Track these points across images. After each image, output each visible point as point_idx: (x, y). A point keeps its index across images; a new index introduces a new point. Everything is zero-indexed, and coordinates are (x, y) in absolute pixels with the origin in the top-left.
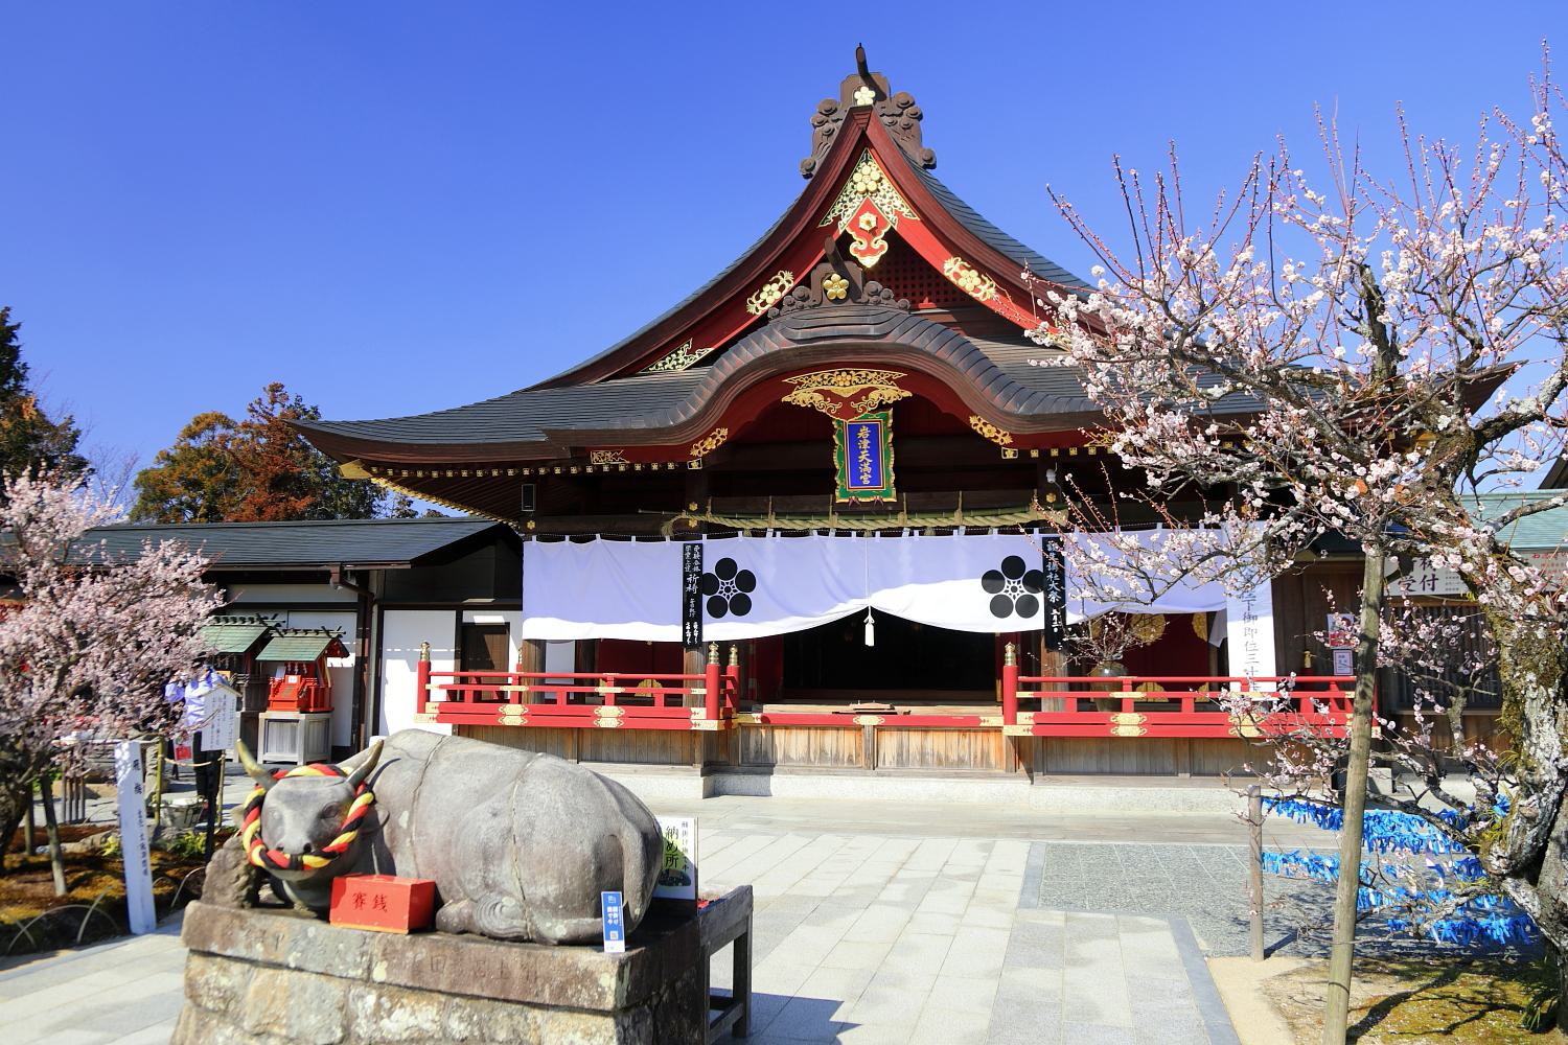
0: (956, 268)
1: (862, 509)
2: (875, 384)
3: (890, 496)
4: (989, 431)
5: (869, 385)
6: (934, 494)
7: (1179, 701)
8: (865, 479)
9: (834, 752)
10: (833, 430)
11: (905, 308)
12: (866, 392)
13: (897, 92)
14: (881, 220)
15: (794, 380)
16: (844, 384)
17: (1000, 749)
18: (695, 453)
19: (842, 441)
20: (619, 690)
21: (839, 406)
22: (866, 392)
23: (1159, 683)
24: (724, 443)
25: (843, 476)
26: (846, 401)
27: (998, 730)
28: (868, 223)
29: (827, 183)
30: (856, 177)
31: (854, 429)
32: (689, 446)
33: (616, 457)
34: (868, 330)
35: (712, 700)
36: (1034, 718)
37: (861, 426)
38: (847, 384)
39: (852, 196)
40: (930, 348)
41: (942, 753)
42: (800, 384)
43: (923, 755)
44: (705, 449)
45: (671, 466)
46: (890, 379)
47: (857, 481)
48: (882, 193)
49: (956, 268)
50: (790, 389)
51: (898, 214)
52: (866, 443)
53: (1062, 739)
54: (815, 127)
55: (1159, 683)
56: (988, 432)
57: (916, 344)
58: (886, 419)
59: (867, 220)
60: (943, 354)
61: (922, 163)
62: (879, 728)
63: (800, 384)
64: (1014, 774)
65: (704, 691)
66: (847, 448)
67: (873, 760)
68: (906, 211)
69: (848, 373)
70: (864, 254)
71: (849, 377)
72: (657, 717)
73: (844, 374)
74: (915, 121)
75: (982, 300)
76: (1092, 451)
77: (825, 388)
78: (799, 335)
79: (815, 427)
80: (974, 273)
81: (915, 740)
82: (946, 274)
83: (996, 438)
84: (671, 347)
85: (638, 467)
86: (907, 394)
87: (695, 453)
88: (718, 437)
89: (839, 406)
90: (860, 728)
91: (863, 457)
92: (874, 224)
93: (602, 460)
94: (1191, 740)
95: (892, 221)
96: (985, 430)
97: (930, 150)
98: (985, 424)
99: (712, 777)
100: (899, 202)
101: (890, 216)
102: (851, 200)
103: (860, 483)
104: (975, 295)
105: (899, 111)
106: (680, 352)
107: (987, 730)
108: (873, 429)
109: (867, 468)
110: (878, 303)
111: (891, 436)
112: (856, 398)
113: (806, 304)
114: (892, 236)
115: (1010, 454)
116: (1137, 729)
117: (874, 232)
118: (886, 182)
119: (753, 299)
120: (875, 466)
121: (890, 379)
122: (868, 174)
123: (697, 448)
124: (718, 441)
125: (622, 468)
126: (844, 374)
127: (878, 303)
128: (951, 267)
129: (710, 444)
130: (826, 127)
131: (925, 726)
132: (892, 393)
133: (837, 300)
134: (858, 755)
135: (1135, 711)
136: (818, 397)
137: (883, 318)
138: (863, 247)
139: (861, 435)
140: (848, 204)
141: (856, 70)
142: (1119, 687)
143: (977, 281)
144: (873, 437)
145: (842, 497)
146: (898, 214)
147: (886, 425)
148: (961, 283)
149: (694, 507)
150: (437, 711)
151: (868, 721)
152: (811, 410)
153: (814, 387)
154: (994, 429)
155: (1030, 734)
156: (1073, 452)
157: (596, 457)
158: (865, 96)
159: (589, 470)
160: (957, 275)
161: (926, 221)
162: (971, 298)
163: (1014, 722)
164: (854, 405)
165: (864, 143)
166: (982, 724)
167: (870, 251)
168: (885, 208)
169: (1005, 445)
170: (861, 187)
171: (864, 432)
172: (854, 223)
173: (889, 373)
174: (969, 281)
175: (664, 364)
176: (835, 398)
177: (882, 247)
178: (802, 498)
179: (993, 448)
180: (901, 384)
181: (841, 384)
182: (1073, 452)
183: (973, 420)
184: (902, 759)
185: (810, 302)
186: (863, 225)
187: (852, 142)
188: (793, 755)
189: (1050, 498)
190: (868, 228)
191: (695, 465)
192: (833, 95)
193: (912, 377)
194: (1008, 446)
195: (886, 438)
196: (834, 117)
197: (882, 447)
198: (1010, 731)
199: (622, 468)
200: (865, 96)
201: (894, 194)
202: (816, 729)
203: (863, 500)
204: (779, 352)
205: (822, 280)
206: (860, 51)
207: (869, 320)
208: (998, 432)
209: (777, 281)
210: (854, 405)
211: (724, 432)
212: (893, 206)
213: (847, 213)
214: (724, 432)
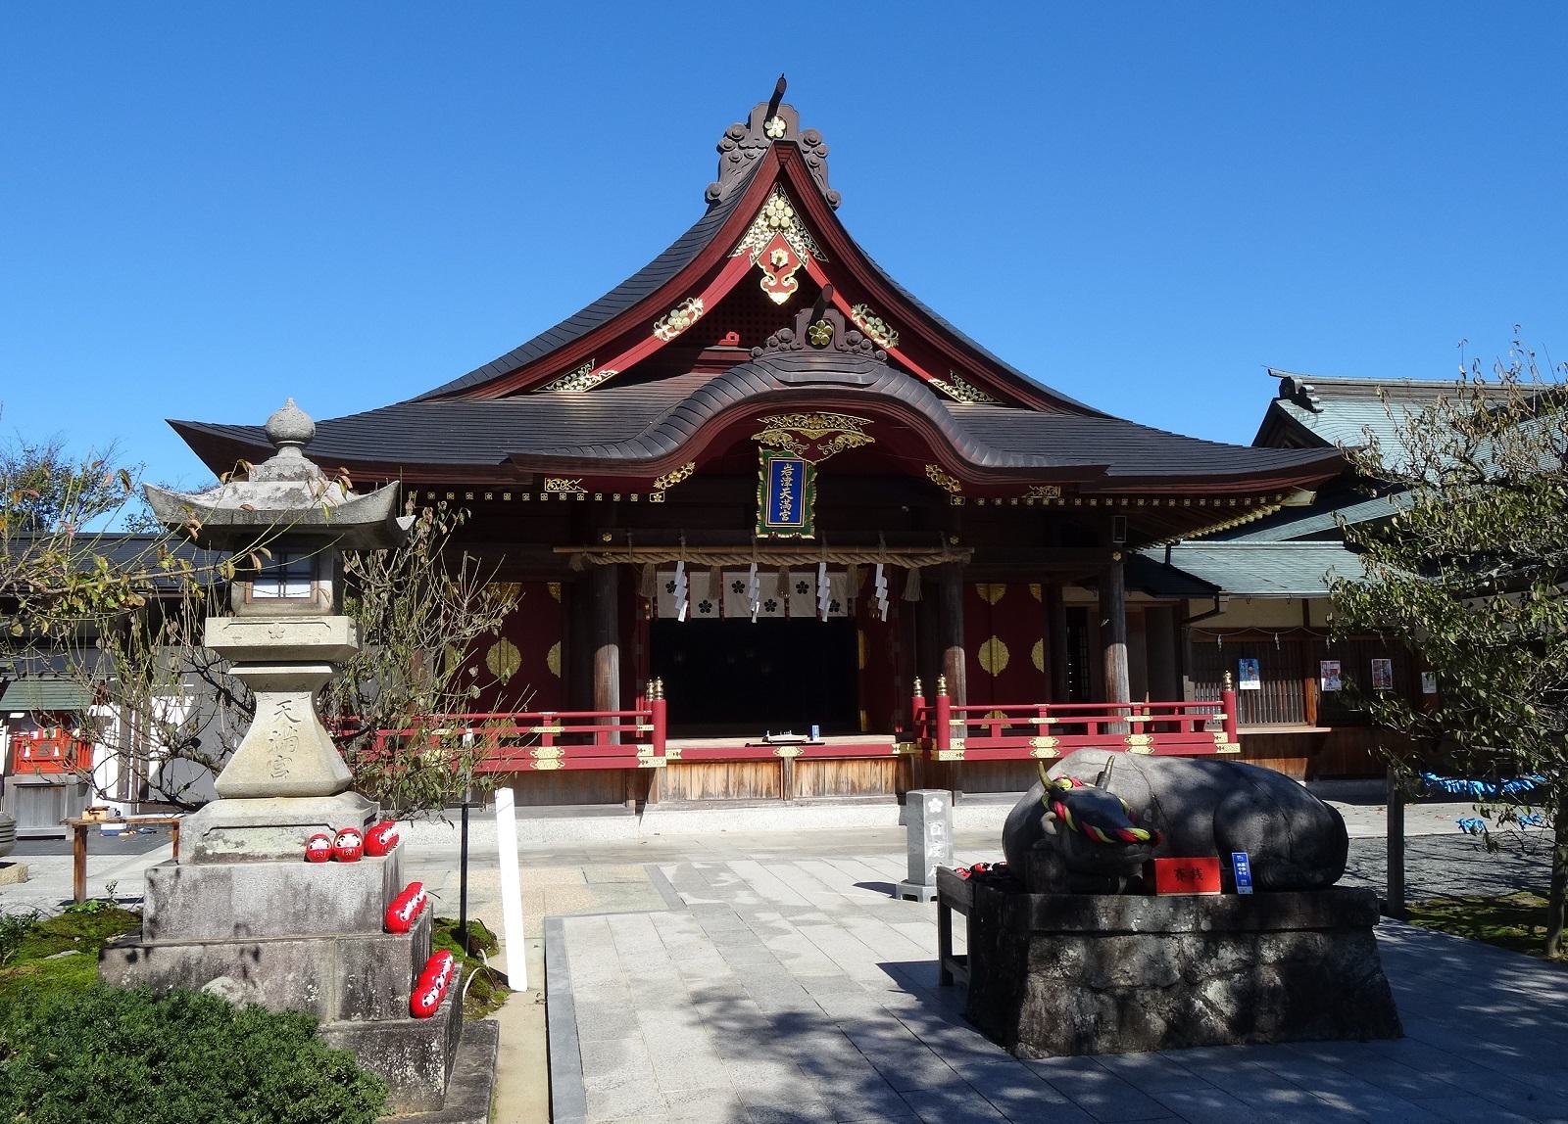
7: (591, 734)
8: (785, 515)
9: (753, 785)
10: (758, 467)
12: (834, 435)
18: (658, 485)
19: (765, 476)
20: (1053, 720)
22: (834, 435)
23: (1004, 711)
26: (814, 443)
28: (779, 259)
31: (779, 466)
33: (573, 485)
43: (837, 782)
44: (669, 483)
47: (776, 517)
50: (762, 427)
52: (788, 481)
55: (1004, 711)
62: (798, 760)
63: (772, 423)
67: (782, 790)
70: (772, 289)
76: (1030, 502)
81: (830, 770)
84: (572, 369)
85: (599, 498)
86: (871, 440)
87: (658, 485)
90: (779, 761)
91: (784, 494)
93: (558, 487)
101: (801, 254)
103: (779, 519)
104: (695, 318)
108: (797, 467)
109: (787, 505)
112: (824, 440)
114: (801, 275)
115: (958, 501)
119: (660, 323)
120: (795, 503)
124: (684, 474)
125: (581, 498)
129: (676, 477)
131: (842, 758)
135: (554, 745)
138: (772, 283)
142: (539, 722)
145: (761, 533)
150: (963, 747)
151: (788, 752)
155: (963, 758)
156: (1015, 502)
159: (544, 497)
167: (779, 288)
169: (955, 493)
171: (788, 470)
176: (803, 439)
177: (792, 286)
179: (940, 493)
183: (928, 468)
184: (818, 791)
188: (711, 790)
190: (774, 261)
191: (657, 498)
194: (957, 494)
195: (809, 479)
197: (804, 485)
202: (735, 763)
203: (783, 536)
204: (768, 393)
206: (782, 83)
207: (855, 368)
209: (888, 331)
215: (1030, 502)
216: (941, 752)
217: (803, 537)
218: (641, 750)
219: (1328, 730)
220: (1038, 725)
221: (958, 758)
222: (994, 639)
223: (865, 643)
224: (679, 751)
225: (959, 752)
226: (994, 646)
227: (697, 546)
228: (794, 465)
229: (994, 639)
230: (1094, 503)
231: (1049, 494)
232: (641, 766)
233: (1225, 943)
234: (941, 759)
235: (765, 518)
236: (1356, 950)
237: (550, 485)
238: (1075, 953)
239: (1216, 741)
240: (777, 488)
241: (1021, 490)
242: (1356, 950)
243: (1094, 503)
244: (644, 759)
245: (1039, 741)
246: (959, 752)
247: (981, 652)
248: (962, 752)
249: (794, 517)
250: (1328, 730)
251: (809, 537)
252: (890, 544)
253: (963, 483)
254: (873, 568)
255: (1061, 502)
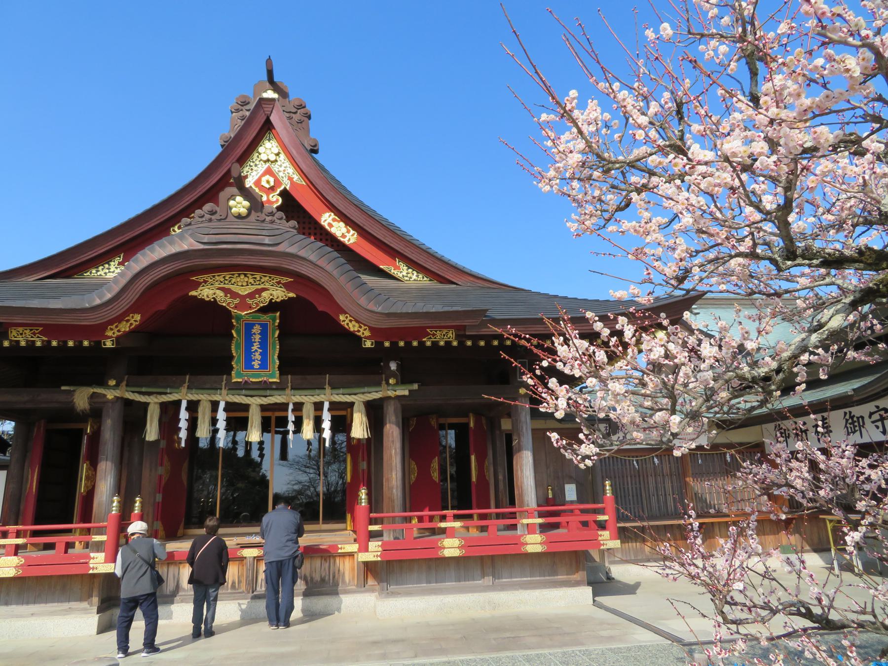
0: (330, 220)
1: (252, 387)
2: (267, 286)
3: (274, 378)
4: (354, 326)
5: (259, 287)
6: (308, 377)
8: (256, 364)
10: (232, 326)
11: (294, 228)
13: (294, 95)
14: (278, 182)
15: (200, 278)
16: (242, 285)
17: (353, 569)
18: (109, 333)
19: (238, 333)
21: (237, 301)
22: (259, 292)
24: (137, 326)
25: (238, 362)
27: (351, 555)
28: (268, 182)
29: (240, 148)
30: (261, 149)
32: (103, 327)
34: (264, 240)
35: (110, 547)
36: (381, 546)
37: (254, 324)
38: (245, 284)
39: (257, 162)
40: (313, 257)
41: (308, 575)
42: (205, 282)
45: (86, 343)
46: (279, 283)
47: (249, 365)
48: (279, 163)
49: (330, 220)
50: (196, 285)
51: (290, 179)
52: (257, 338)
53: (400, 561)
54: (232, 112)
56: (353, 327)
57: (302, 253)
58: (274, 319)
59: (267, 181)
60: (322, 263)
61: (309, 148)
64: (363, 589)
65: (104, 538)
66: (242, 341)
68: (296, 177)
69: (245, 275)
71: (246, 279)
72: (51, 561)
73: (242, 276)
74: (306, 119)
75: (347, 243)
76: (429, 344)
77: (226, 286)
78: (206, 239)
79: (217, 318)
80: (342, 224)
82: (322, 223)
83: (359, 331)
86: (292, 295)
87: (109, 333)
88: (132, 321)
89: (237, 301)
90: (242, 559)
91: (254, 348)
92: (272, 184)
93: (21, 337)
94: (493, 556)
95: (286, 185)
96: (351, 325)
97: (315, 140)
98: (351, 321)
99: (108, 613)
100: (291, 170)
102: (256, 165)
103: (252, 367)
104: (342, 239)
105: (295, 110)
106: (112, 263)
107: (344, 555)
108: (264, 327)
109: (258, 356)
110: (272, 222)
111: (277, 332)
112: (251, 295)
113: (213, 217)
114: (285, 194)
115: (368, 344)
116: (458, 551)
117: (272, 189)
118: (282, 156)
120: (264, 355)
121: (279, 283)
122: (269, 148)
123: (112, 329)
124: (131, 324)
125: (39, 344)
126: (242, 276)
127: (272, 222)
128: (327, 219)
129: (125, 327)
130: (240, 114)
132: (279, 294)
133: (239, 217)
134: (239, 582)
136: (220, 294)
137: (277, 232)
139: (254, 331)
140: (254, 168)
141: (265, 77)
143: (344, 230)
144: (264, 334)
145: (237, 377)
146: (290, 179)
147: (273, 324)
148: (333, 230)
149: (112, 383)
150: (380, 549)
152: (213, 304)
153: (217, 285)
154: (357, 325)
155: (379, 559)
156: (415, 344)
157: (14, 333)
158: (270, 94)
160: (330, 225)
161: (311, 183)
162: (339, 241)
163: (367, 550)
164: (249, 301)
165: (267, 127)
166: (340, 551)
168: (281, 174)
169: (365, 337)
170: (264, 157)
172: (258, 183)
173: (278, 278)
174: (339, 230)
175: (98, 271)
176: (234, 295)
177: (277, 200)
178: (205, 378)
179: (356, 339)
180: (288, 286)
181: (240, 284)
182: (415, 344)
183: (342, 318)
185: (217, 217)
186: (264, 183)
187: (256, 128)
189: (391, 381)
190: (267, 186)
191: (109, 344)
192: (249, 93)
193: (299, 280)
195: (274, 334)
196: (247, 107)
197: (270, 340)
198: (364, 557)
199: (39, 344)
200: (270, 94)
201: (287, 163)
203: (254, 380)
205: (229, 200)
206: (269, 62)
208: (360, 327)
210: (249, 301)
211: (138, 317)
212: (287, 173)
213: (253, 174)
214: (138, 317)
215: (429, 344)
217: (271, 380)
220: (446, 528)
227: (339, 388)
228: (262, 325)
230: (482, 343)
231: (445, 337)
232: (91, 572)
235: (237, 365)
237: (13, 334)
238: (562, 451)
239: (600, 538)
240: (249, 343)
241: (421, 332)
243: (482, 343)
244: (95, 566)
245: (448, 542)
249: (264, 365)
251: (275, 380)
252: (334, 387)
253: (371, 329)
254: (178, 403)
255: (455, 344)
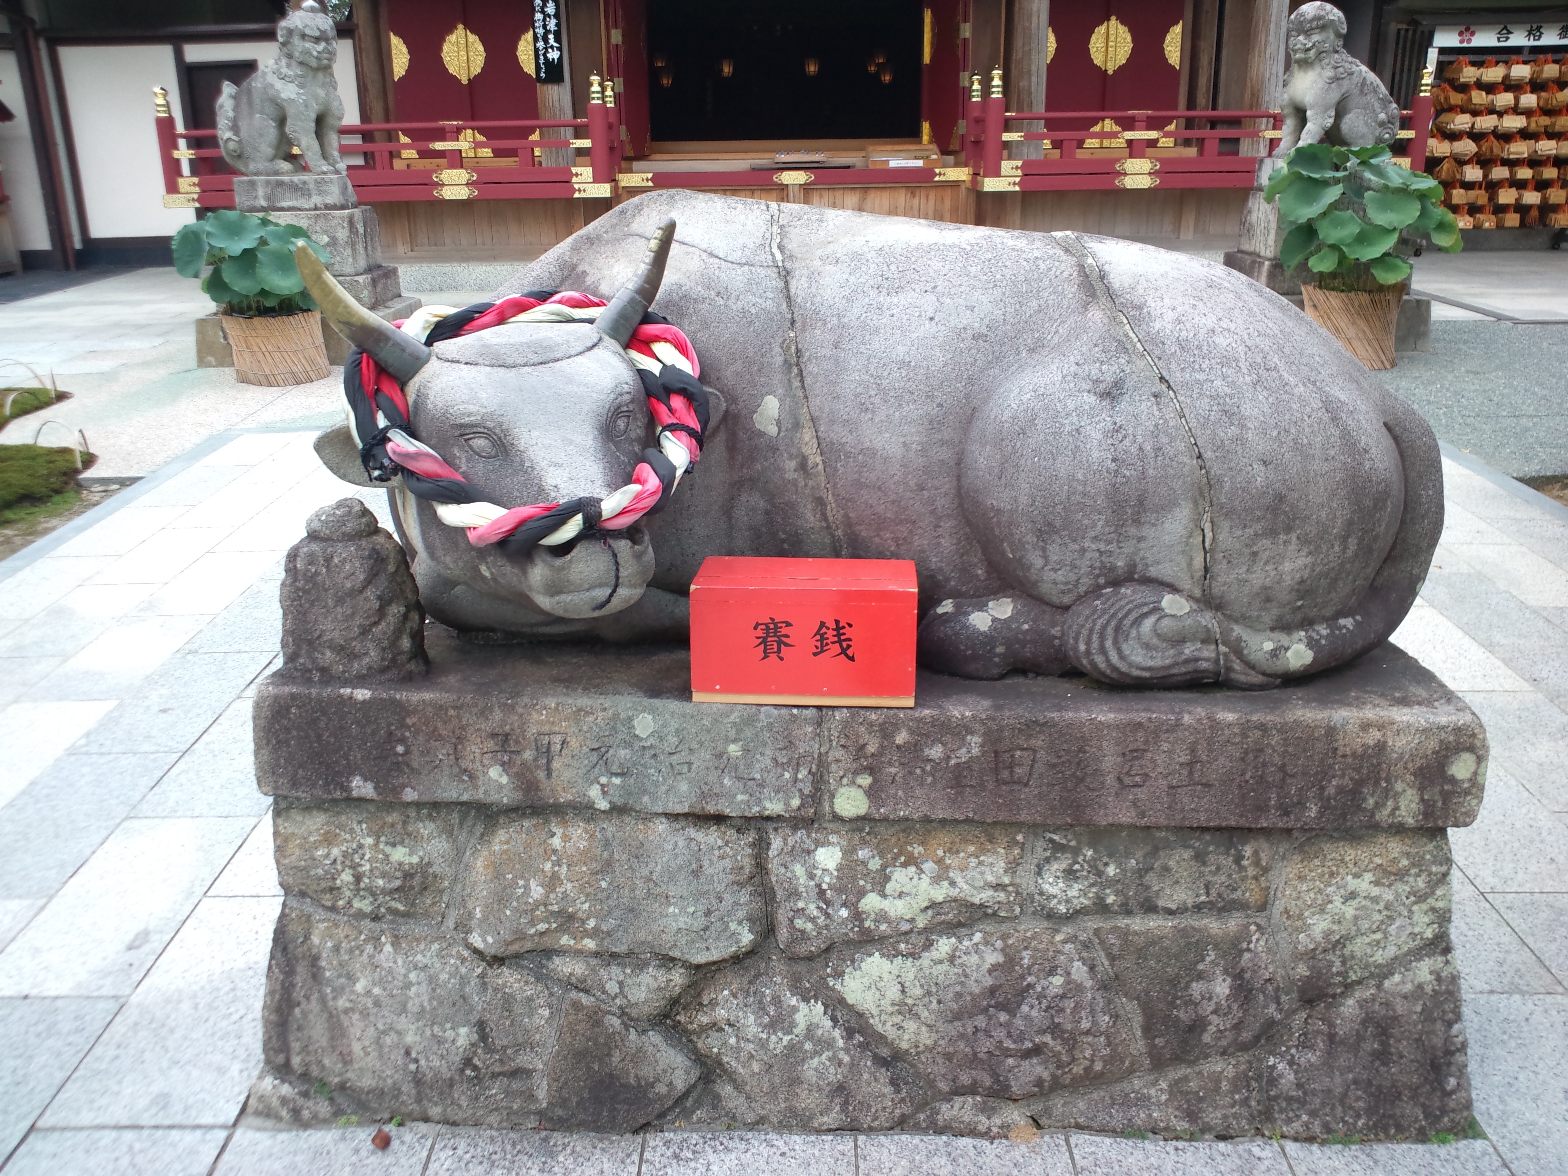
150: (1019, 173)
216: (986, 180)
218: (577, 175)
219: (927, 58)
221: (1011, 188)
222: (1113, 21)
223: (932, 23)
224: (650, 176)
225: (1012, 180)
226: (1112, 31)
229: (1113, 21)
233: (918, 850)
234: (986, 189)
236: (1375, 891)
242: (1375, 891)
244: (582, 186)
246: (1012, 180)
247: (1094, 38)
248: (1017, 180)
250: (927, 58)
